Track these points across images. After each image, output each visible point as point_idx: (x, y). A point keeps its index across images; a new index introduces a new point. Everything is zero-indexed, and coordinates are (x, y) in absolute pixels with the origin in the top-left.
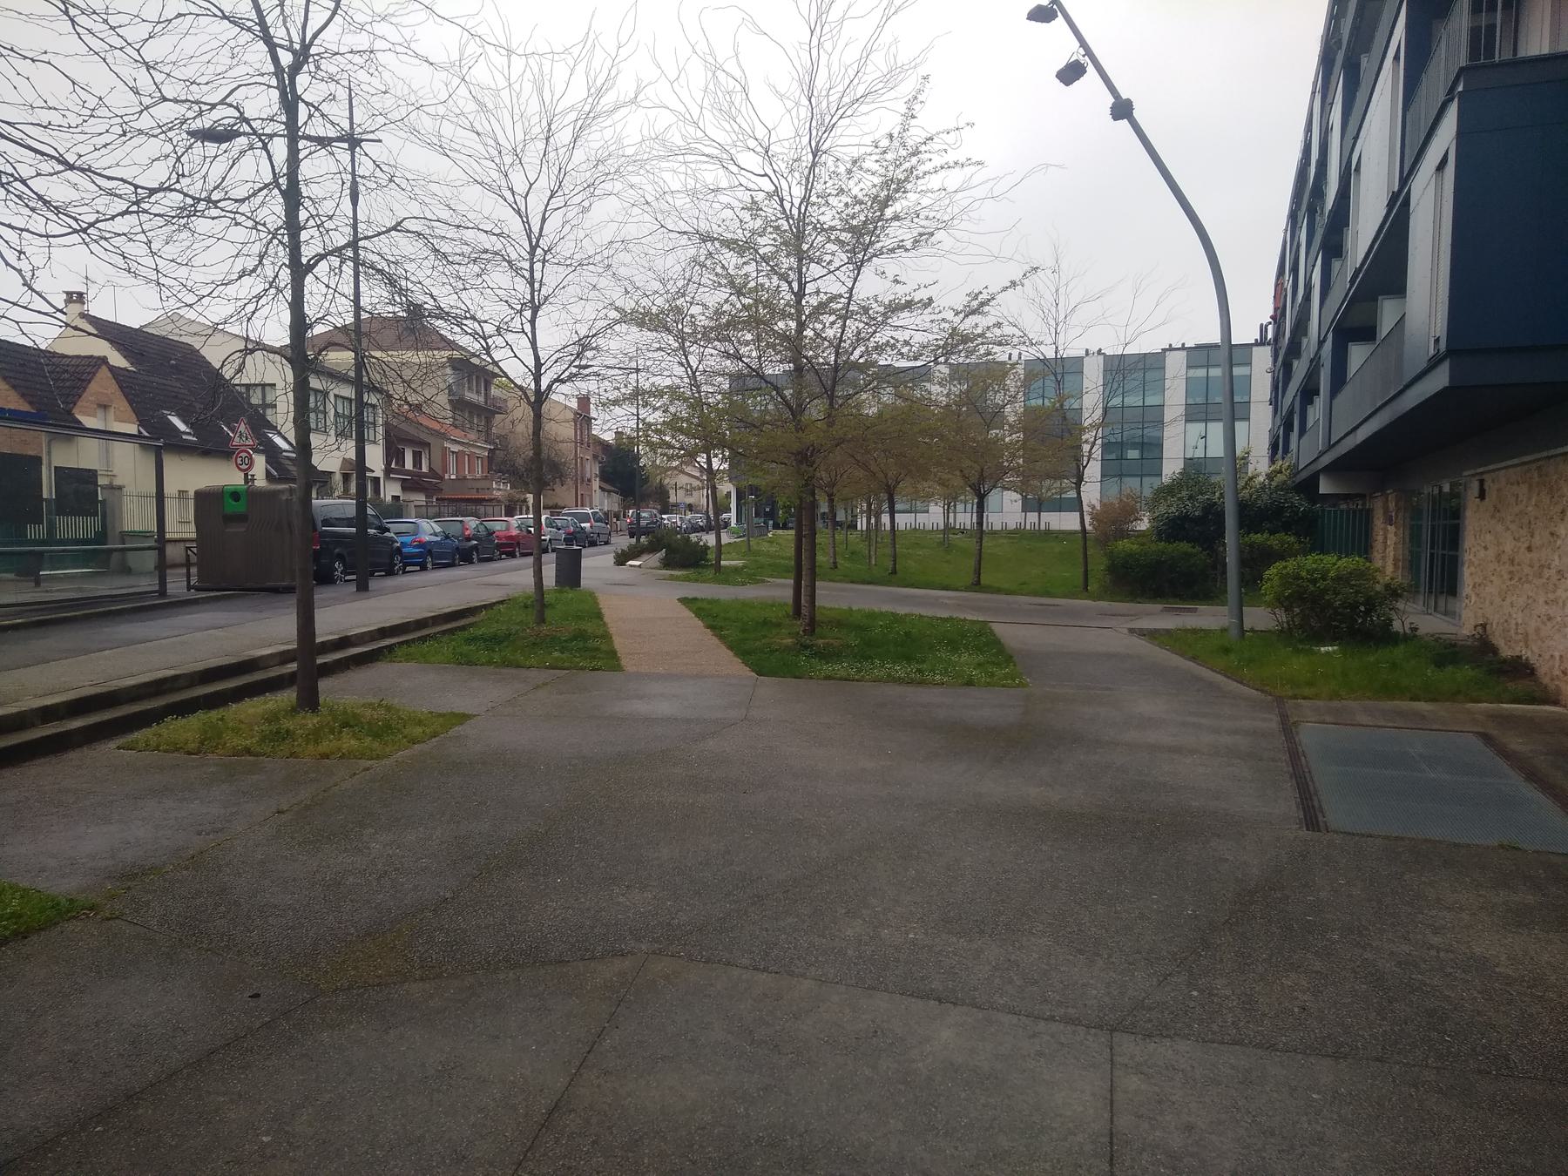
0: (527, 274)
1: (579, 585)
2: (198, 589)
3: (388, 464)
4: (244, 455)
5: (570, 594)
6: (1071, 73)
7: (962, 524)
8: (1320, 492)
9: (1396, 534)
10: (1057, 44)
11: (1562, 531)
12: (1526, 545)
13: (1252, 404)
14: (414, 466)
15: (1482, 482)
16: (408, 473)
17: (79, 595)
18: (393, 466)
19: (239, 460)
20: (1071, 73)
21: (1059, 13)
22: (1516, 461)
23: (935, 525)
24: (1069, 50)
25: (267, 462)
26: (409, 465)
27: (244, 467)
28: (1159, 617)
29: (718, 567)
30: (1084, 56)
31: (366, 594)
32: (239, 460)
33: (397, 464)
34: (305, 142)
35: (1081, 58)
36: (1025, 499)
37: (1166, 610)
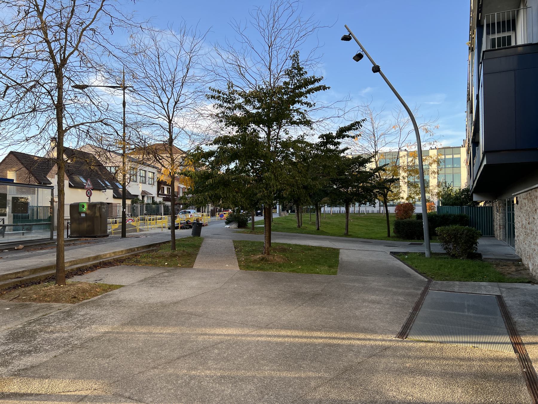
0: (168, 130)
1: (200, 236)
2: (70, 237)
3: (158, 192)
4: (89, 191)
5: (196, 238)
6: (359, 57)
7: (363, 211)
8: (474, 200)
9: (499, 216)
10: (352, 48)
11: (536, 218)
12: (528, 222)
13: (461, 168)
14: (167, 193)
15: (517, 198)
16: (165, 195)
17: (19, 240)
18: (160, 193)
19: (87, 193)
20: (359, 57)
21: (352, 37)
22: (523, 191)
23: (343, 211)
24: (357, 50)
25: (114, 192)
26: (166, 193)
27: (89, 195)
28: (403, 247)
29: (253, 228)
30: (362, 51)
31: (125, 239)
32: (87, 193)
33: (161, 192)
34: (57, 94)
35: (361, 52)
36: (364, 204)
37: (411, 244)
